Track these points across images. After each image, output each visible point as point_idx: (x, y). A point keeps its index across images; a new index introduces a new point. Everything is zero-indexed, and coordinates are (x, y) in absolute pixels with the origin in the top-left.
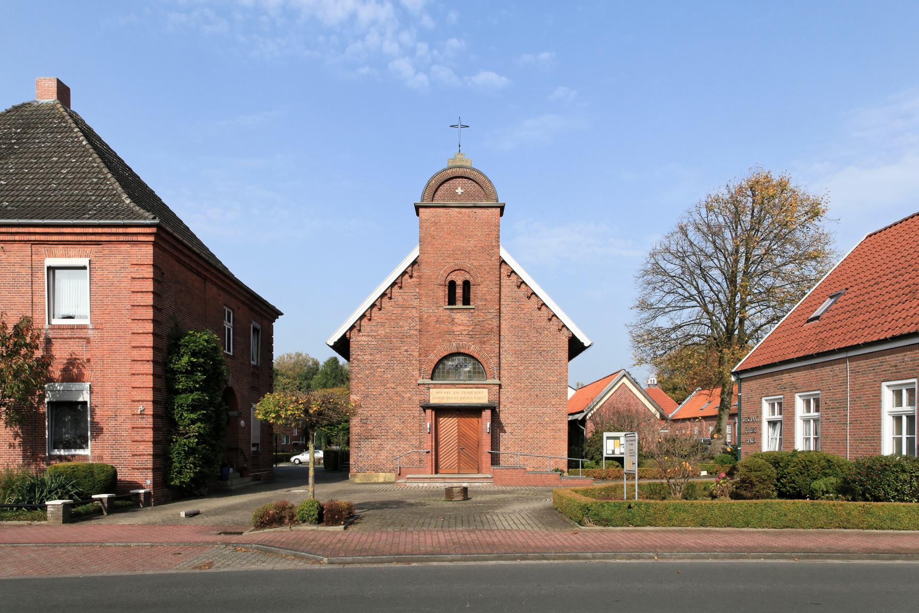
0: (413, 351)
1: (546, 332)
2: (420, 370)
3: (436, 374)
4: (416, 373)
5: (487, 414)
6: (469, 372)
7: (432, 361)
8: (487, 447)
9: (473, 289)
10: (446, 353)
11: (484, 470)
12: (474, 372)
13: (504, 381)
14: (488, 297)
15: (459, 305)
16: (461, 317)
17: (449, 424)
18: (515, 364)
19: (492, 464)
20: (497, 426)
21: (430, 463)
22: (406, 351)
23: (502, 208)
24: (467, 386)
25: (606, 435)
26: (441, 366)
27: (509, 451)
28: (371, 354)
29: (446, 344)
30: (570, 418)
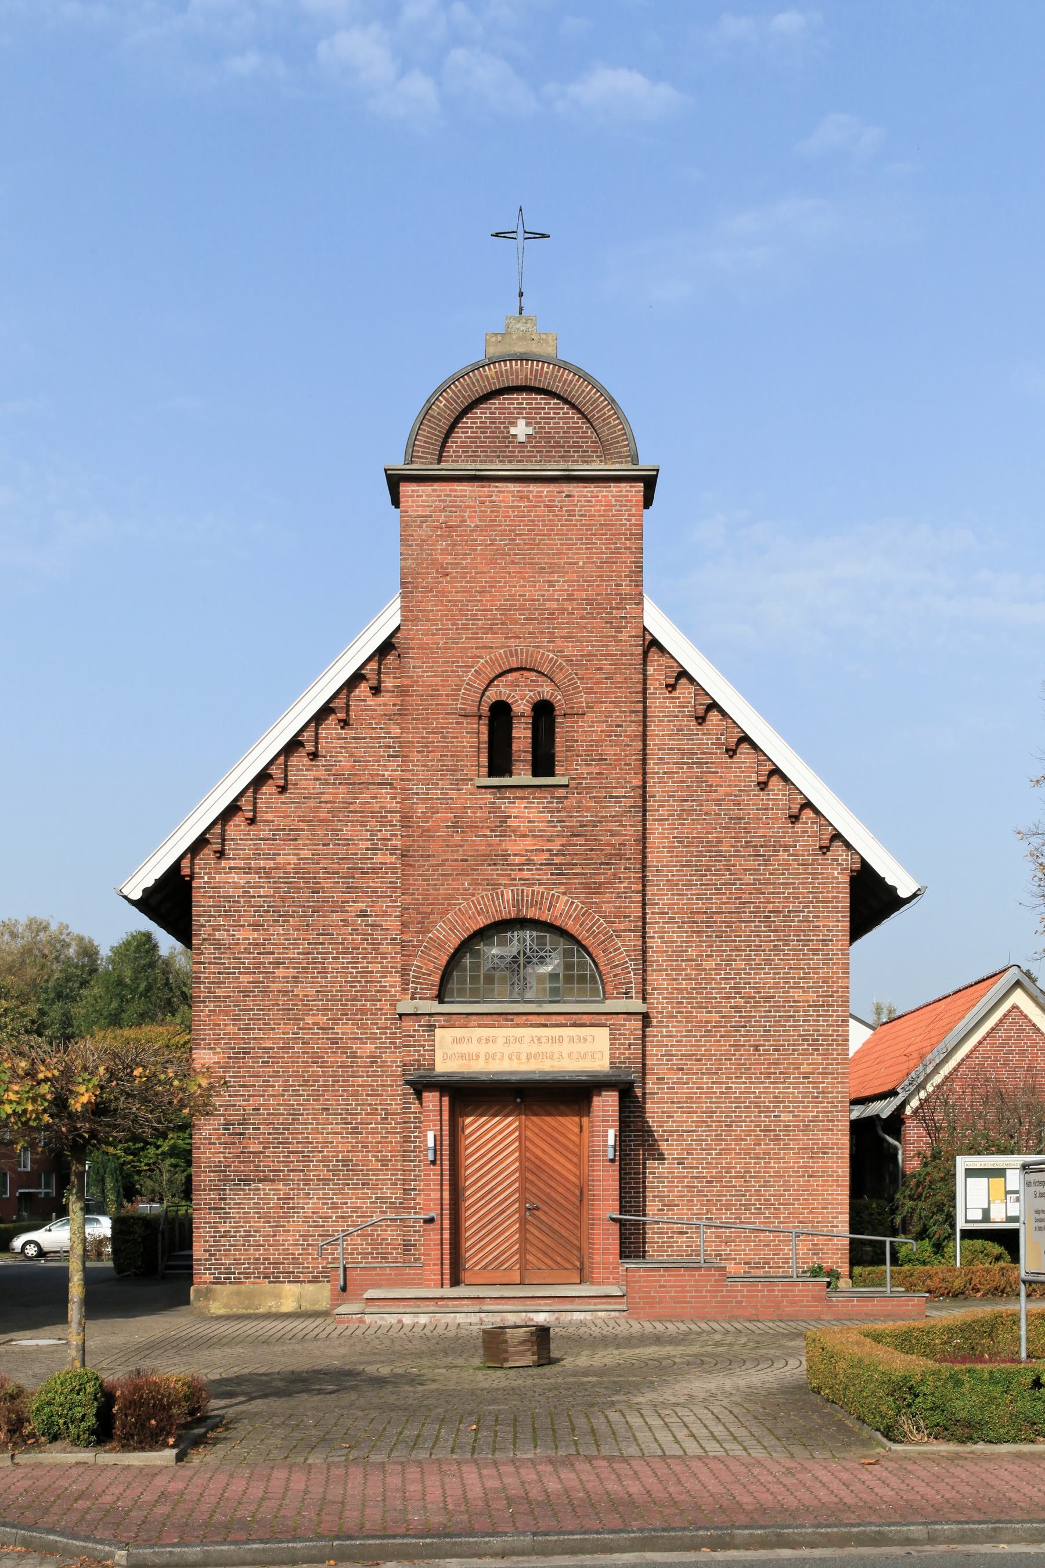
0: (385, 914)
1: (783, 856)
2: (404, 972)
3: (454, 985)
5: (607, 1104)
6: (553, 976)
9: (562, 728)
10: (482, 922)
11: (599, 1273)
13: (659, 1003)
14: (610, 752)
15: (523, 776)
16: (528, 813)
17: (491, 1135)
19: (624, 1254)
21: (435, 1255)
22: (363, 914)
23: (649, 482)
25: (963, 1163)
26: (578, 1264)
28: (256, 926)
30: (447, 1282)
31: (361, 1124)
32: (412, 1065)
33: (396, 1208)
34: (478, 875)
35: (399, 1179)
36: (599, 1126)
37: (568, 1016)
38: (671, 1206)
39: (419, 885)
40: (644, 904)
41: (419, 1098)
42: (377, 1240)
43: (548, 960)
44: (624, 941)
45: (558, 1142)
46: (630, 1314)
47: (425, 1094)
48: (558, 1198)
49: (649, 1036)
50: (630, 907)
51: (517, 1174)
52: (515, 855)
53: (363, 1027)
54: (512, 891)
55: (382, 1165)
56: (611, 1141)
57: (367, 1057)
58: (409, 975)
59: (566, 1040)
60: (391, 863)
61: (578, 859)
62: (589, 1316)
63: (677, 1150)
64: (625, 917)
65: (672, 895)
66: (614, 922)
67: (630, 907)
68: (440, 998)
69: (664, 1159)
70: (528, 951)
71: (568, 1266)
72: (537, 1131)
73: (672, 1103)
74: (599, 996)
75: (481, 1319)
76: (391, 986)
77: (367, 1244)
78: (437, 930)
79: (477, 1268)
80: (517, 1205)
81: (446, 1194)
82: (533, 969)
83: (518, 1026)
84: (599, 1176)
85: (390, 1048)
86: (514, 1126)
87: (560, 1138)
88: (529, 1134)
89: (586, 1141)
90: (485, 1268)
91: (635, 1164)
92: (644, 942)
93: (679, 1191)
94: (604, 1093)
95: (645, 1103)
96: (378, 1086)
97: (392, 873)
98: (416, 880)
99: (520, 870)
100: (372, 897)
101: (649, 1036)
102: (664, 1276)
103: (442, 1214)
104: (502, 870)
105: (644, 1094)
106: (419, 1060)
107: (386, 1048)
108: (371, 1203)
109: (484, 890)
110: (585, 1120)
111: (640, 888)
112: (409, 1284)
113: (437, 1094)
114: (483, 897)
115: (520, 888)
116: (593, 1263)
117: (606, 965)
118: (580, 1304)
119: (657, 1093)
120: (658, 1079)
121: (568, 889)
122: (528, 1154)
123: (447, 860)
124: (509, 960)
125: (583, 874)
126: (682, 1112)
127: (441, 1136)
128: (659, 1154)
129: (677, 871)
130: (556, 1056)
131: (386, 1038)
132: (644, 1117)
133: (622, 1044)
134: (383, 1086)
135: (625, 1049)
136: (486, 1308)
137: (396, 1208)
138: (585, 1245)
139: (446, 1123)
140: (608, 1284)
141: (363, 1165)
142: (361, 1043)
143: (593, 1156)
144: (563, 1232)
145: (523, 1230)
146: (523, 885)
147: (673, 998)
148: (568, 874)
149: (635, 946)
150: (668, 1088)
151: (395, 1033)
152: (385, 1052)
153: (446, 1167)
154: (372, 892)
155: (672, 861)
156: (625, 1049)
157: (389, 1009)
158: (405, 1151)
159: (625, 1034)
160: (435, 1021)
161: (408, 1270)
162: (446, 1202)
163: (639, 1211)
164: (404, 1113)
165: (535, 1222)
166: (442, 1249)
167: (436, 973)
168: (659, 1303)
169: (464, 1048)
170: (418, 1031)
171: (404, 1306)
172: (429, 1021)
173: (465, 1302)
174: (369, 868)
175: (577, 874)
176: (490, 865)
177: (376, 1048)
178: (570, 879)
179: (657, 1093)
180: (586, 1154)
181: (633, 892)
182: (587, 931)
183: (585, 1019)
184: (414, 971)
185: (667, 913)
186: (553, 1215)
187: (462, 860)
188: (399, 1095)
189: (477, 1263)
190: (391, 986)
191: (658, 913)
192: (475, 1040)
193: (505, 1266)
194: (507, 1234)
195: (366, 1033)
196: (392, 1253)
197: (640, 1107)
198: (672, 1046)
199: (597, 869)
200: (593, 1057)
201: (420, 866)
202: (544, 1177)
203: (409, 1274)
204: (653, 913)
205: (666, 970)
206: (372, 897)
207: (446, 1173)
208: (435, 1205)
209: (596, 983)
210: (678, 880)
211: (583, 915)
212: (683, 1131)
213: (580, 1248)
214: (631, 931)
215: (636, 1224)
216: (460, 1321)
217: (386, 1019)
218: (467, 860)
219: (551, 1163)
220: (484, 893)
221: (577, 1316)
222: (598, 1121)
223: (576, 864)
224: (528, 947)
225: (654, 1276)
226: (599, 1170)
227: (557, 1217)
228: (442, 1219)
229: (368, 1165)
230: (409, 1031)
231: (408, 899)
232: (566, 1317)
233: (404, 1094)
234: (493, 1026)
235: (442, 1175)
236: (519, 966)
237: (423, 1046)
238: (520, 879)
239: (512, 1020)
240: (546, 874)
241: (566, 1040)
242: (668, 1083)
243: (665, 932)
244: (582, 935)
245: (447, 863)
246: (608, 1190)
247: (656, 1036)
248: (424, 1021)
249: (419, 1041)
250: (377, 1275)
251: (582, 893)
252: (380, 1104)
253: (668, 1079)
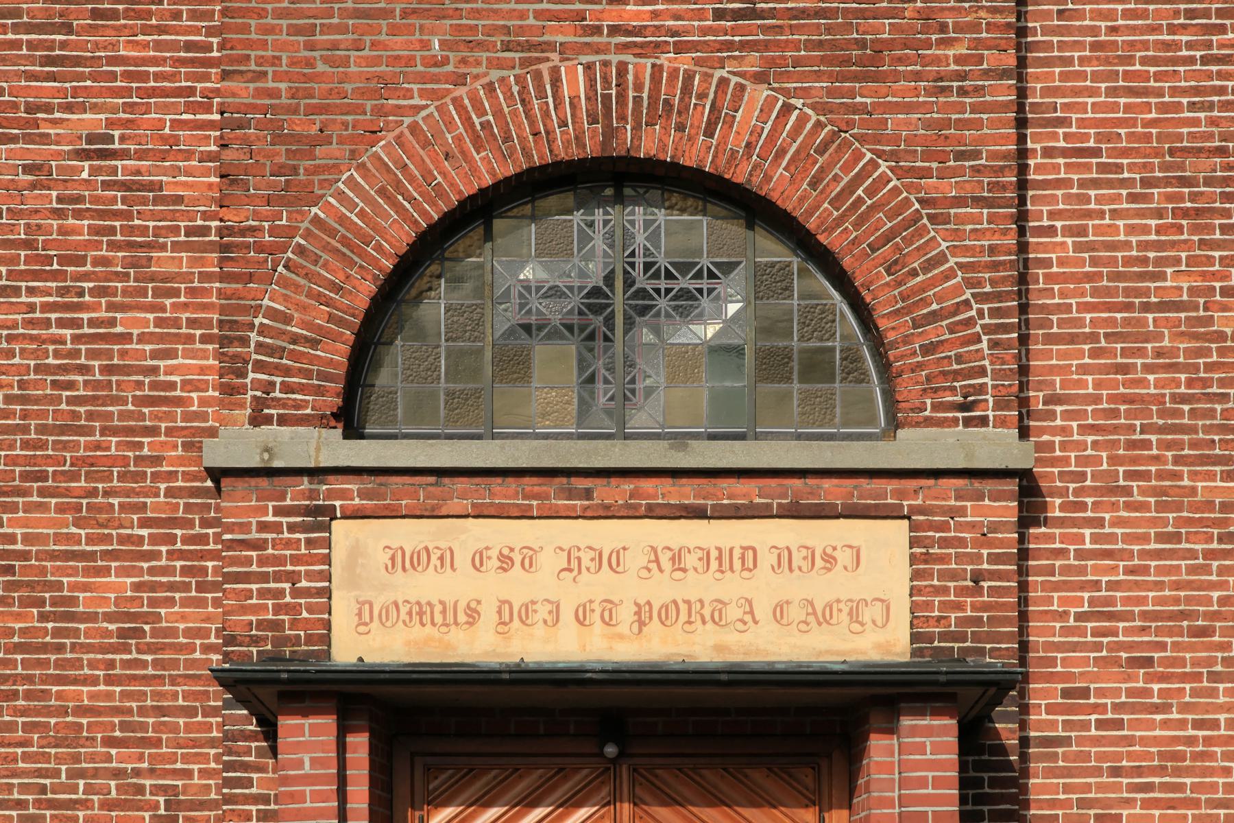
0: (168, 150)
2: (229, 335)
3: (392, 374)
4: (194, 364)
6: (724, 352)
7: (351, 246)
10: (488, 169)
12: (773, 365)
13: (1069, 448)
18: (1176, 283)
22: (97, 149)
24: (698, 491)
53: (96, 517)
59: (767, 559)
241: (767, 559)
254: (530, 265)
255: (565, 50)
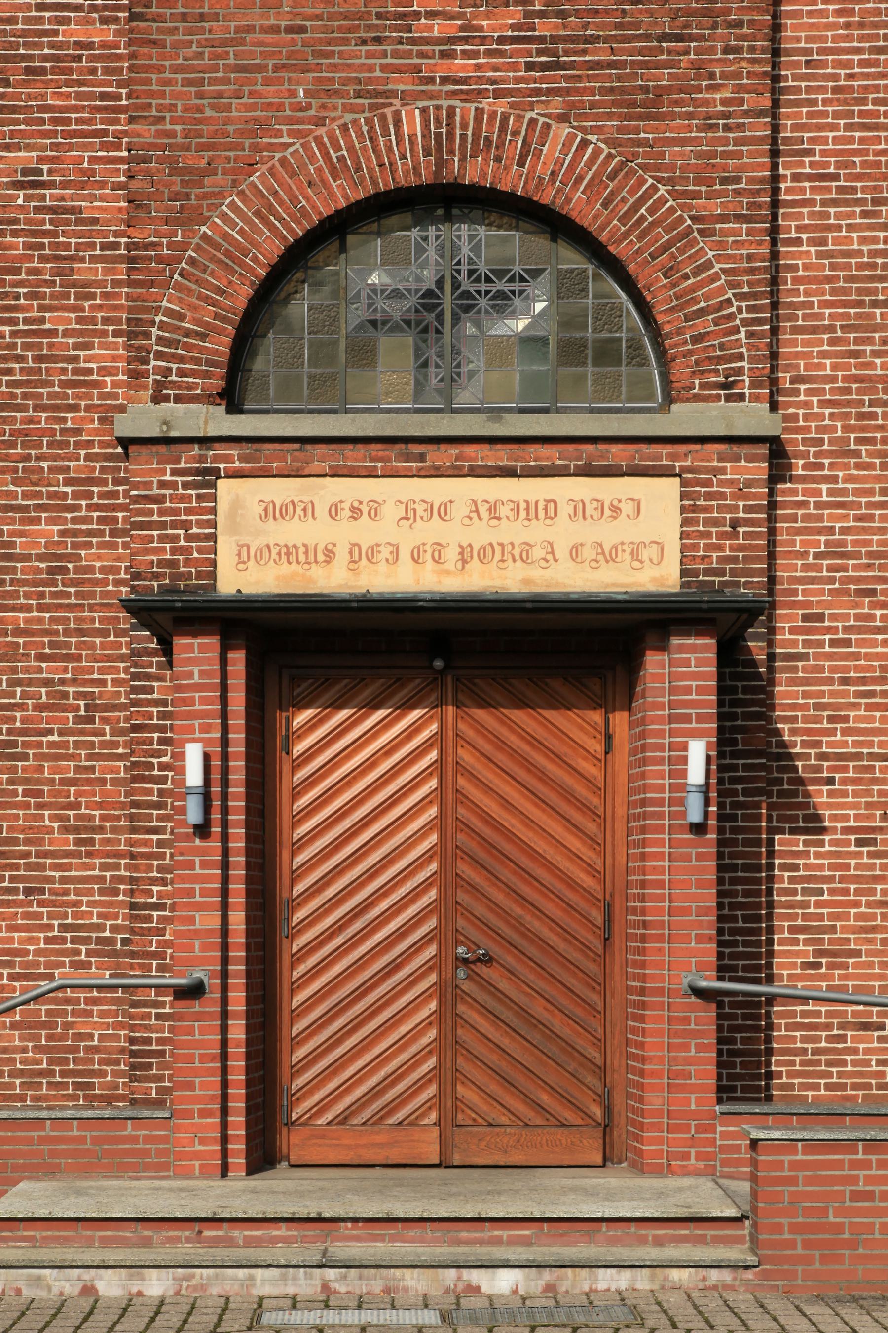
0: (85, 180)
2: (135, 330)
3: (264, 362)
4: (106, 354)
5: (683, 669)
6: (531, 342)
8: (684, 957)
10: (342, 194)
11: (656, 1143)
12: (571, 352)
13: (811, 418)
17: (367, 762)
19: (725, 1091)
20: (759, 782)
21: (206, 1086)
27: (850, 977)
29: (347, 117)
30: (238, 1161)
31: (23, 732)
32: (156, 576)
33: (115, 954)
34: (334, 67)
35: (121, 880)
36: (660, 734)
37: (570, 448)
38: (838, 954)
39: (176, 96)
40: (775, 154)
41: (167, 649)
42: (63, 1037)
43: (517, 301)
44: (722, 245)
45: (543, 777)
46: (766, 1275)
47: (180, 642)
48: (546, 933)
49: (785, 505)
50: (739, 155)
51: (434, 867)
52: (431, 15)
53: (31, 477)
54: (424, 111)
55: (78, 842)
56: (696, 773)
57: (41, 558)
58: (147, 335)
59: (565, 510)
60: (104, 45)
61: (598, 26)
62: (643, 1281)
63: (855, 806)
64: (724, 181)
65: (849, 127)
66: (697, 195)
67: (739, 155)
68: (232, 398)
69: (823, 830)
70: (463, 278)
71: (569, 1116)
72: (487, 748)
73: (845, 681)
74: (651, 397)
75: (325, 1287)
76: (102, 371)
77: (37, 1049)
78: (224, 217)
79: (322, 1121)
80: (432, 950)
81: (238, 919)
82: (478, 325)
83: (437, 473)
84: (661, 870)
85: (101, 533)
86: (425, 734)
87: (551, 768)
88: (466, 756)
89: (622, 778)
90: (343, 1119)
91: (746, 843)
92: (775, 255)
93: (859, 917)
94: (675, 641)
95: (772, 682)
96: (67, 633)
97: (107, 71)
98: (168, 82)
99: (444, 55)
100: (53, 134)
101: (785, 505)
102: (867, 1165)
103: (225, 974)
104: (396, 54)
105: (771, 657)
106: (173, 564)
107: (90, 533)
108: (48, 941)
109: (352, 109)
110: (619, 720)
111: (766, 102)
112: (134, 1167)
113: (213, 641)
114: (344, 128)
115: (445, 103)
116: (642, 1113)
117: (672, 310)
118: (614, 1241)
119: (804, 657)
120: (806, 618)
121: (572, 105)
122: (462, 811)
123: (250, 29)
124: (412, 301)
125: (611, 65)
126: (870, 707)
127: (225, 757)
128: (807, 818)
129: (862, 63)
130: (538, 553)
131: (90, 508)
132: (769, 720)
133: (716, 523)
134: (81, 633)
135: (721, 535)
136: (341, 1250)
137: (115, 954)
138: (616, 1061)
139: (238, 721)
140: (686, 1172)
141: (27, 842)
142: (23, 521)
143: (645, 816)
144: (557, 1023)
145: (447, 1018)
146: (453, 94)
147: (849, 403)
148: (572, 65)
149: (750, 258)
150: (833, 643)
151: (114, 495)
152: (89, 545)
153: (238, 844)
154: (55, 121)
155: (848, 38)
156: (721, 535)
157: (97, 432)
158: (135, 804)
159: (723, 496)
160: (216, 459)
161: (129, 1129)
162: (238, 938)
163: (758, 968)
164: (135, 703)
165: (482, 996)
166: (224, 1070)
167: (221, 332)
168: (852, 1244)
169: (292, 531)
170: (173, 485)
171: (106, 1243)
172: (202, 459)
173: (282, 1231)
174: (45, 58)
175: (598, 65)
176: (364, 42)
177: (62, 533)
178: (578, 78)
179: (804, 657)
180: (621, 811)
181: (746, 114)
182: (623, 220)
183: (617, 454)
184: (162, 326)
185: (835, 177)
186: (531, 977)
187: (290, 29)
188: (122, 658)
189: (322, 1108)
190: (102, 371)
191: (810, 178)
192: (322, 511)
193: (400, 1115)
194: (404, 1029)
195: (39, 495)
196: (102, 1074)
197: (762, 690)
198: (844, 531)
199: (650, 51)
200: (635, 555)
201: (176, 45)
202: (506, 874)
203: (134, 1139)
204: (796, 177)
205: (831, 329)
206: (53, 134)
207: (238, 859)
208: (205, 947)
209: (644, 362)
210: (866, 89)
211: (611, 178)
212: (872, 756)
213: (604, 1069)
214: (739, 218)
215: (751, 1003)
216: (266, 1290)
217: (88, 457)
218: (302, 29)
219: (526, 835)
220: (348, 117)
221: (608, 1280)
222: (660, 720)
223: (595, 39)
224: (464, 268)
225: (839, 1165)
226: (660, 856)
227: (540, 985)
228: (225, 988)
229: (40, 842)
230: (148, 485)
231: (146, 132)
232: (575, 1283)
233: (135, 653)
234: (371, 474)
235: (225, 865)
236: (440, 318)
237: (186, 525)
238: (445, 80)
239: (422, 458)
240: (514, 67)
241: (565, 510)
242: (834, 630)
243: (829, 228)
244: (609, 230)
245: (249, 37)
246: (686, 911)
247: (803, 504)
248: (188, 457)
249: (176, 512)
250: (42, 1140)
251: (610, 116)
252: (74, 682)
253: (833, 617)
254: (375, 272)
255: (406, 98)
